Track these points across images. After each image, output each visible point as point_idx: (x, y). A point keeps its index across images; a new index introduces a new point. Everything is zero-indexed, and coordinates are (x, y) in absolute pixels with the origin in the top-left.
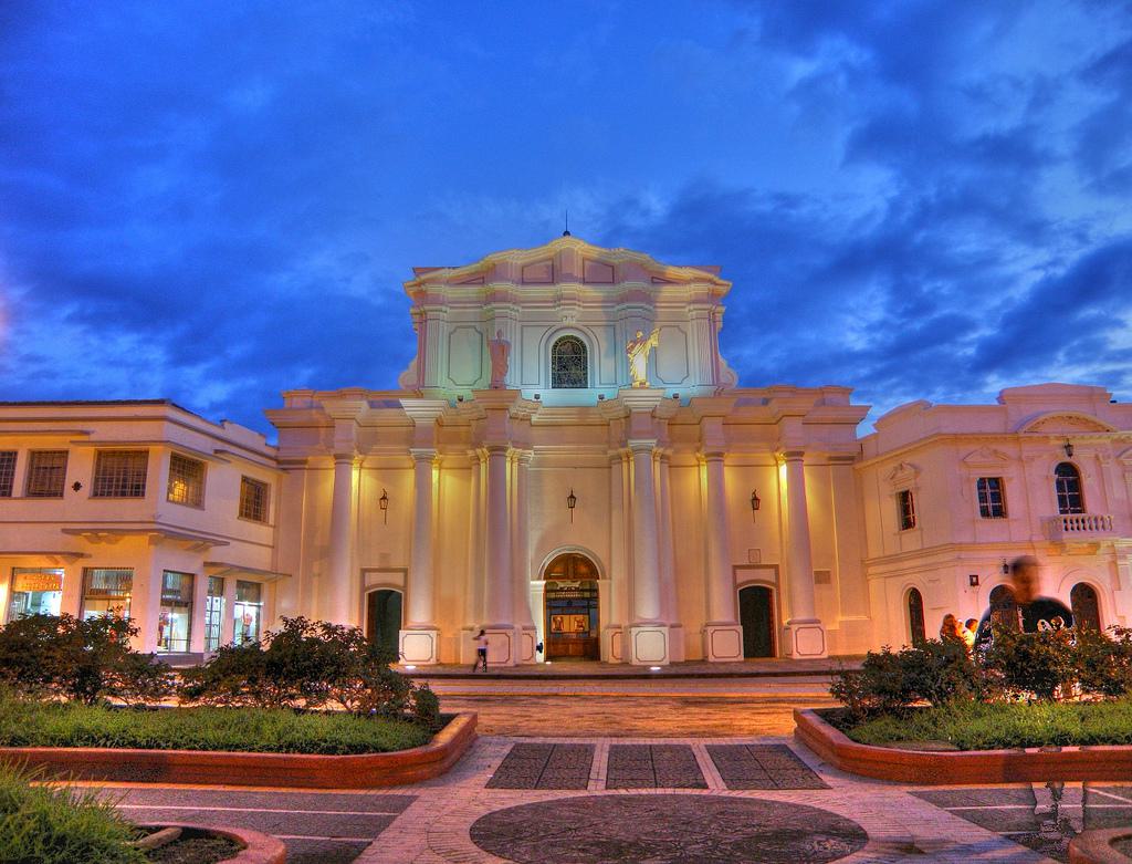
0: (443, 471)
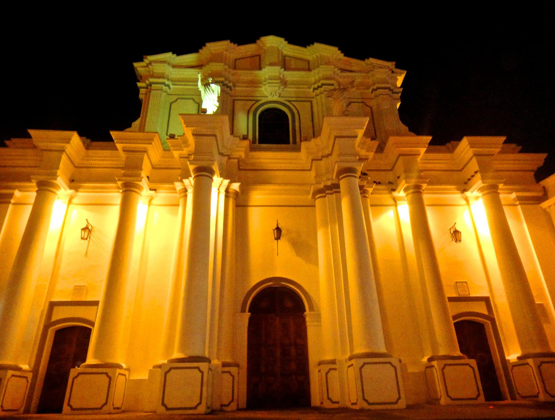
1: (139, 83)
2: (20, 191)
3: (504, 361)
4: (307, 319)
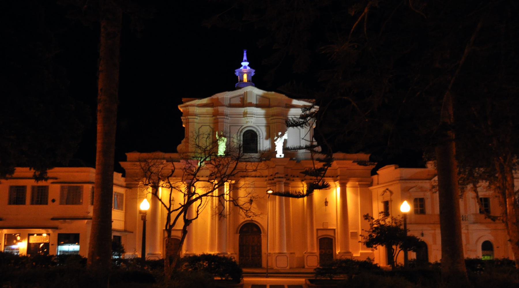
3: (336, 253)
4: (262, 236)
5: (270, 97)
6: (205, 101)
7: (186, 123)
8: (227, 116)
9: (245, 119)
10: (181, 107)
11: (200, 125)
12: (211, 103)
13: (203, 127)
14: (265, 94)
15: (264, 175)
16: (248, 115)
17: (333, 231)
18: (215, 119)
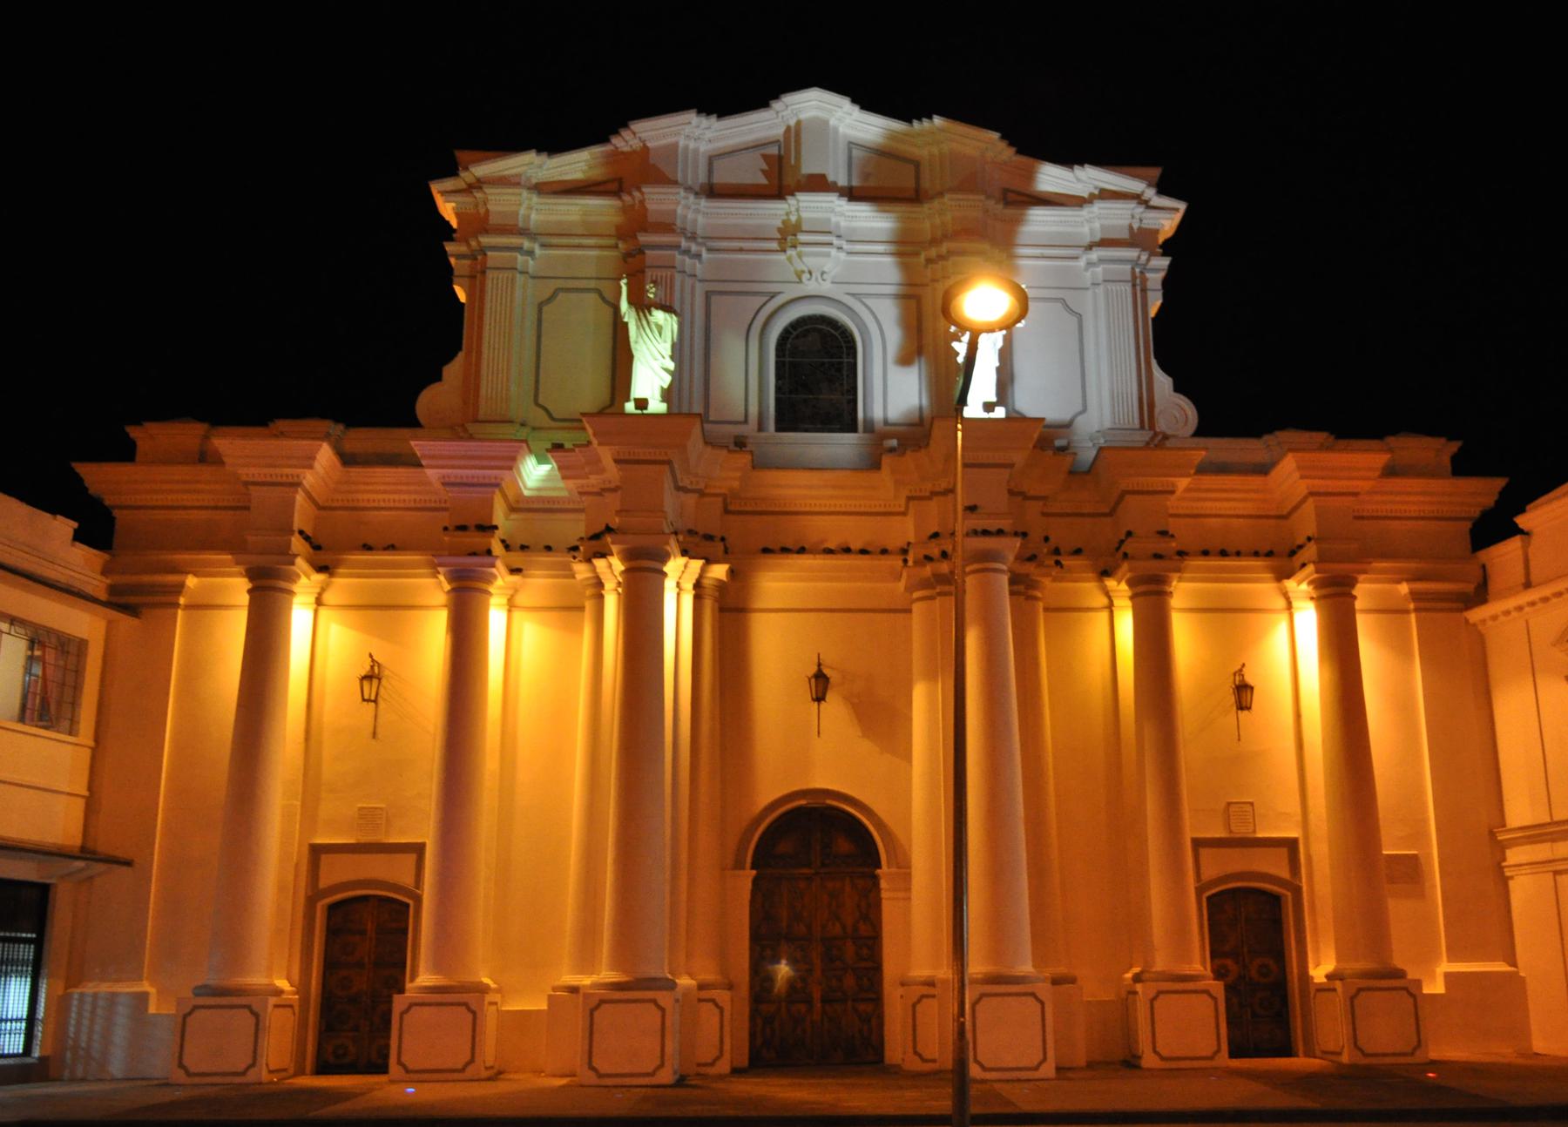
0: (517, 615)
1: (452, 243)
2: (196, 575)
3: (1305, 977)
4: (883, 884)
5: (921, 152)
6: (577, 164)
7: (472, 277)
8: (693, 237)
9: (790, 259)
10: (443, 193)
11: (548, 288)
12: (614, 180)
13: (561, 296)
14: (893, 136)
15: (895, 543)
16: (802, 237)
17: (1284, 851)
18: (628, 255)
